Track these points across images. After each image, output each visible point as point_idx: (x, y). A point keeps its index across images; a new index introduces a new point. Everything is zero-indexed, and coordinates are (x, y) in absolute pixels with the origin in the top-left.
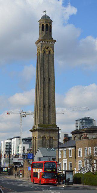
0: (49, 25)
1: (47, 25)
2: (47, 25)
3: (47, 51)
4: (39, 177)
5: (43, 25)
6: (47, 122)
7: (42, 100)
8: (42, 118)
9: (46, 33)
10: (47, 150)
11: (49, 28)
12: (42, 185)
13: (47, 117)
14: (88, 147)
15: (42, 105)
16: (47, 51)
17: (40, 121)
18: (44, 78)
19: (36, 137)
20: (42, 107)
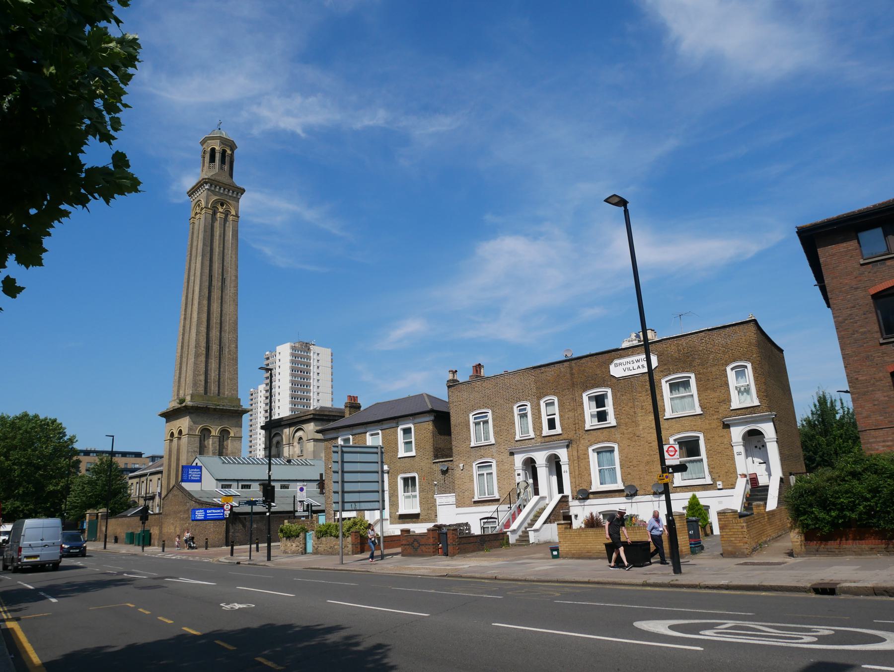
0: (229, 152)
1: (224, 152)
2: (224, 152)
3: (221, 210)
4: (716, 531)
5: (213, 150)
6: (213, 388)
7: (203, 329)
8: (202, 378)
9: (221, 168)
10: (224, 463)
11: (227, 159)
12: (879, 598)
13: (213, 375)
14: (540, 398)
15: (203, 344)
16: (221, 210)
17: (195, 384)
18: (211, 277)
19: (180, 432)
20: (203, 350)
